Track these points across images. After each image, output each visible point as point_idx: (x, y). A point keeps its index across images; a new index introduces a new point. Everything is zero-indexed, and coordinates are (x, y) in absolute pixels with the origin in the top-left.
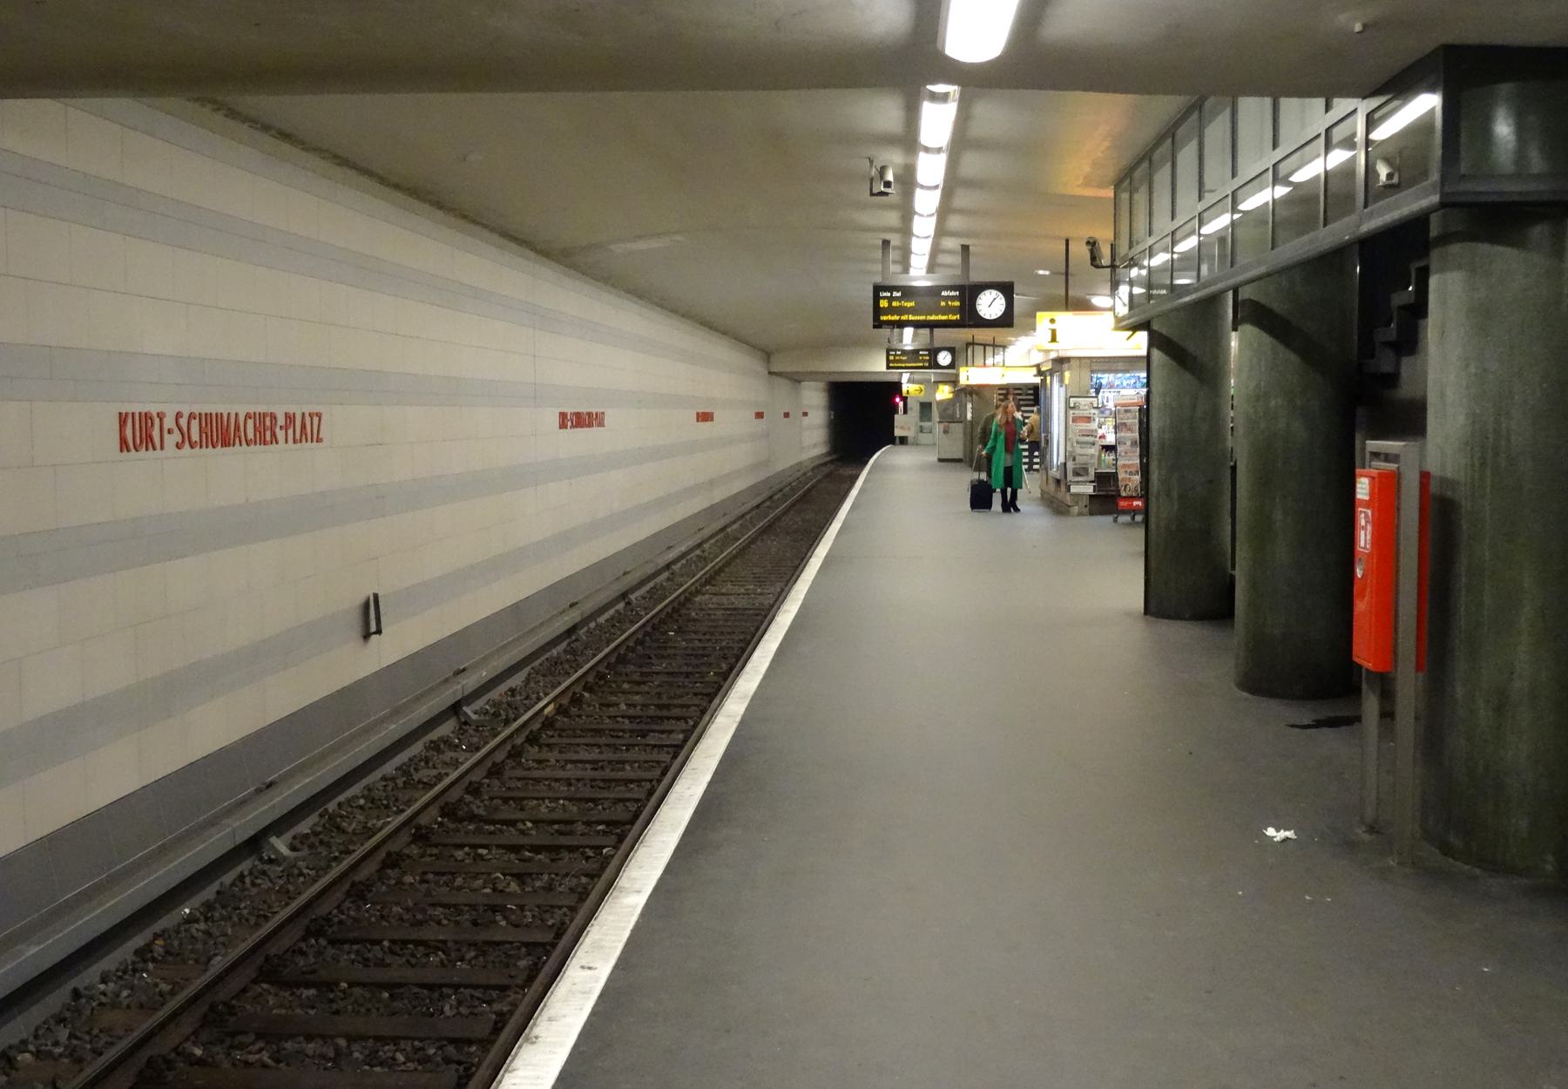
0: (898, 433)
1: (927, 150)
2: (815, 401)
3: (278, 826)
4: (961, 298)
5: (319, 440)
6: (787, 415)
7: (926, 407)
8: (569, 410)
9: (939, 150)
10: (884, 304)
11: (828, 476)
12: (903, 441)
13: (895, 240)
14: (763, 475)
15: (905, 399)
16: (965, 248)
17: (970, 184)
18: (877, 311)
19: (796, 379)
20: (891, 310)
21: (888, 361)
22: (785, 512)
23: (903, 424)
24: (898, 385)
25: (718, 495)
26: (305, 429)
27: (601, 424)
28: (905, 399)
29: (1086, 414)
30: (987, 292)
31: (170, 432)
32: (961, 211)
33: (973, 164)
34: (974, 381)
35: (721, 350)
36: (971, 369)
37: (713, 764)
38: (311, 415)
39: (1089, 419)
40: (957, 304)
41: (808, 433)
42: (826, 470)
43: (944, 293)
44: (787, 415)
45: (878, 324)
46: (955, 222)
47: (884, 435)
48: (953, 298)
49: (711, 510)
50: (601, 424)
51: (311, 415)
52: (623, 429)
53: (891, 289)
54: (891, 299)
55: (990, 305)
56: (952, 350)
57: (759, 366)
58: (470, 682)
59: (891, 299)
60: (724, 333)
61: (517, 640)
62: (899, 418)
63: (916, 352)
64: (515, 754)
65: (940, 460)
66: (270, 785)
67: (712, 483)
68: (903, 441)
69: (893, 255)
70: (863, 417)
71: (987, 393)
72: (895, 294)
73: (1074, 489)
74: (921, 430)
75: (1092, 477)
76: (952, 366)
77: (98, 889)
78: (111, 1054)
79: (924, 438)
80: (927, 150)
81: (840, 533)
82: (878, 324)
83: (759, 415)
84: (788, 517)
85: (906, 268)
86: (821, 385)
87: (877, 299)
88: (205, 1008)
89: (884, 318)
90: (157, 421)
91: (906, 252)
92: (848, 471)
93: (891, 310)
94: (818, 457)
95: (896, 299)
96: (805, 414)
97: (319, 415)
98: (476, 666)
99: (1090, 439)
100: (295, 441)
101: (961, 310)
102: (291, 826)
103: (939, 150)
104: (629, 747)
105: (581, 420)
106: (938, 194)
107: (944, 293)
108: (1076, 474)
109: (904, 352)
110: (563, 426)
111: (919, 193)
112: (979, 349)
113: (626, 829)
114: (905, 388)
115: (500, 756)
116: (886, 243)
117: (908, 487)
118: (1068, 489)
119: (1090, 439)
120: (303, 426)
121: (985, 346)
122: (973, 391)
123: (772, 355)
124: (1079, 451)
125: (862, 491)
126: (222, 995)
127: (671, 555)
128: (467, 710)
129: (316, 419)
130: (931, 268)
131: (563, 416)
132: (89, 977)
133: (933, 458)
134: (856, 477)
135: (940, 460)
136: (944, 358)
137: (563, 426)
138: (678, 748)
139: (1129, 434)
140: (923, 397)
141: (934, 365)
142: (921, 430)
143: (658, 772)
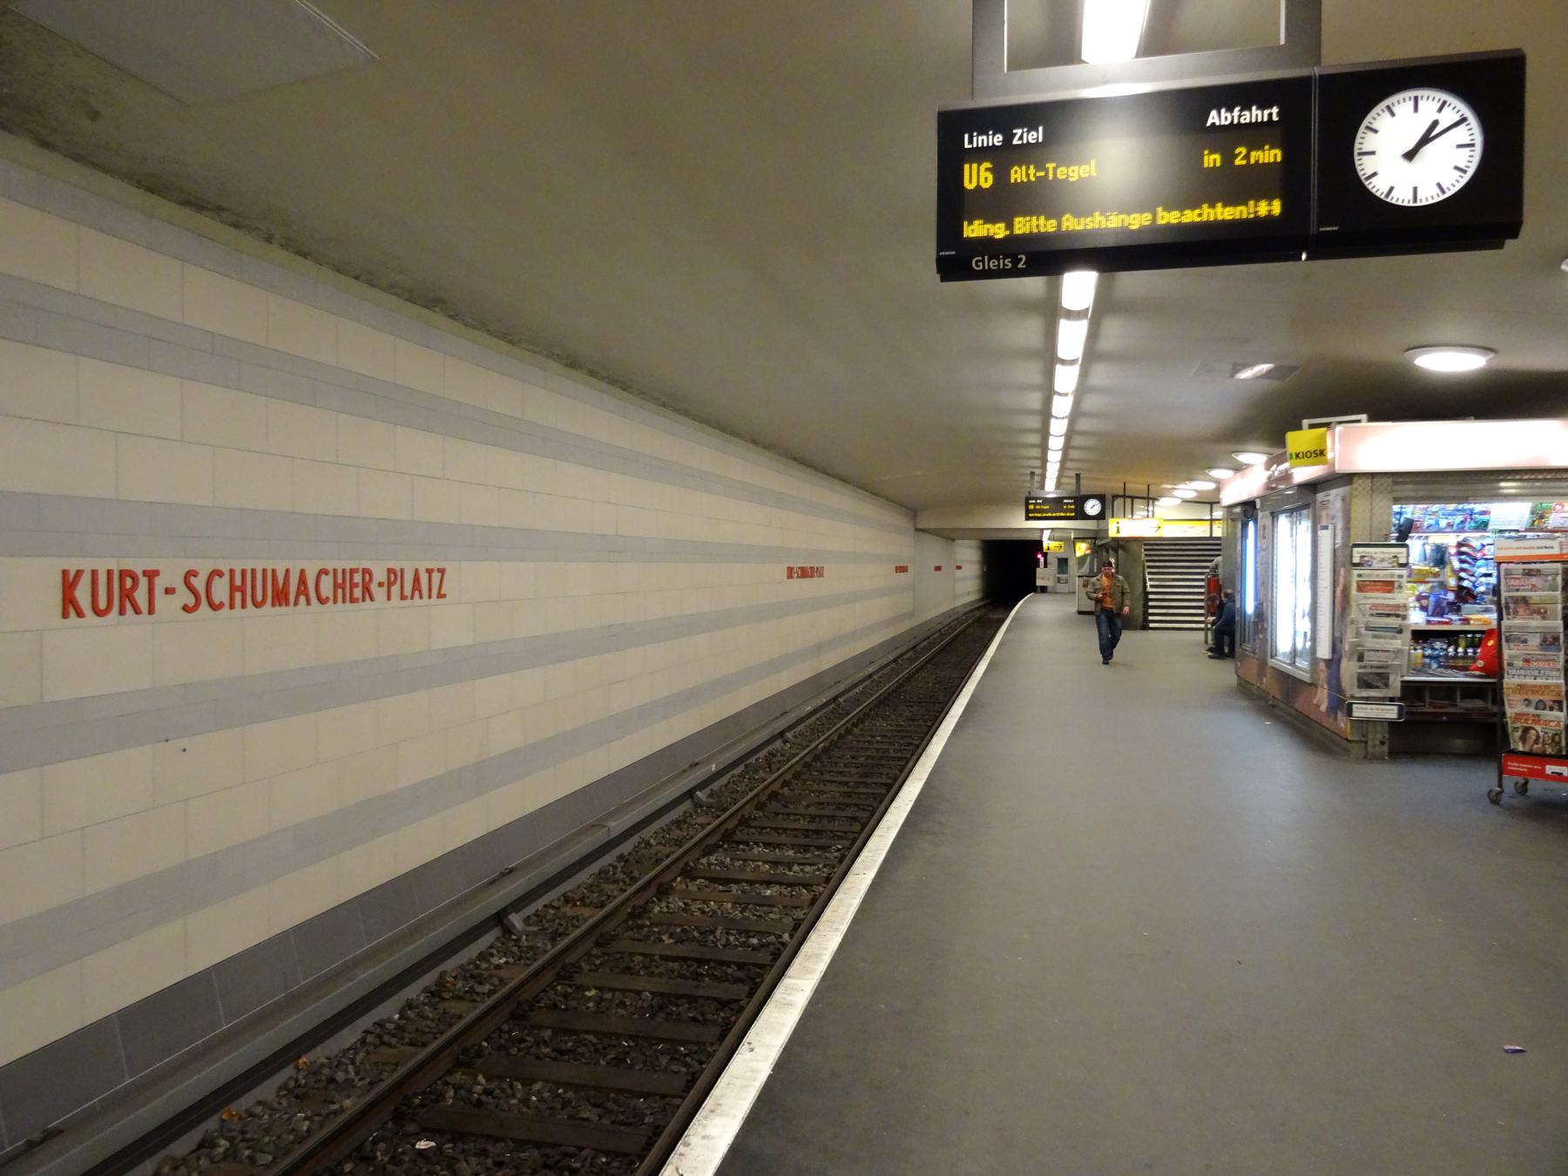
0: (1039, 583)
1: (1063, 362)
2: (969, 559)
3: (701, 786)
4: (1287, 133)
5: (440, 596)
6: (938, 569)
7: (1063, 563)
8: (795, 565)
9: (1073, 362)
10: (978, 177)
11: (979, 620)
12: (1044, 589)
13: (1038, 471)
14: (906, 626)
15: (1045, 555)
16: (1078, 476)
17: (1088, 415)
18: (953, 203)
19: (949, 537)
20: (1035, 511)
21: (1028, 511)
22: (921, 668)
23: (1043, 576)
24: (1040, 542)
25: (828, 661)
26: (422, 586)
27: (821, 575)
28: (1045, 555)
29: (1383, 576)
30: (1402, 103)
31: (169, 591)
32: (1078, 448)
33: (1102, 374)
34: (1124, 534)
35: (868, 509)
36: (1122, 521)
37: (855, 903)
38: (430, 572)
39: (1389, 586)
40: (1270, 155)
41: (962, 582)
42: (978, 614)
43: (1216, 118)
44: (938, 569)
45: (958, 261)
46: (1073, 454)
47: (1027, 585)
48: (1253, 135)
49: (817, 681)
50: (821, 575)
51: (430, 572)
52: (837, 579)
53: (1006, 118)
54: (1002, 158)
55: (1416, 152)
56: (1101, 498)
57: (898, 519)
58: (842, 687)
59: (1002, 158)
60: (844, 480)
61: (669, 781)
62: (1040, 571)
63: (1059, 500)
64: (841, 737)
65: (1080, 613)
66: (50, 1135)
67: (819, 648)
68: (1044, 589)
69: (1037, 478)
70: (1011, 570)
71: (1134, 547)
72: (1022, 136)
73: (1360, 711)
74: (1059, 580)
75: (1395, 689)
76: (1101, 516)
77: (657, 788)
78: (577, 932)
79: (1061, 587)
80: (1063, 362)
81: (958, 726)
82: (958, 261)
83: (902, 569)
84: (918, 678)
85: (1042, 487)
86: (974, 543)
87: (951, 160)
88: (559, 966)
89: (975, 230)
90: (143, 581)
91: (1043, 477)
92: (996, 616)
93: (1035, 511)
94: (971, 603)
95: (1026, 154)
96: (959, 568)
97: (442, 571)
98: (709, 760)
99: (1394, 622)
100: (403, 597)
101: (1286, 180)
102: (437, 965)
103: (1073, 362)
104: (832, 818)
105: (805, 573)
106: (1066, 422)
107: (1216, 118)
108: (1364, 683)
109: (1046, 501)
110: (790, 576)
111: (1059, 368)
112: (1128, 501)
113: (779, 959)
114: (1045, 546)
115: (798, 768)
116: (1033, 474)
117: (1046, 623)
118: (1349, 713)
119: (1394, 622)
120: (417, 580)
121: (1133, 498)
122: (1121, 545)
123: (921, 514)
124: (1370, 642)
125: (1277, 24)
126: (572, 958)
127: (871, 670)
128: (516, 920)
129: (436, 576)
130: (1058, 485)
131: (790, 570)
132: (647, 833)
133: (1074, 609)
134: (1003, 621)
135: (1080, 613)
136: (1092, 507)
137: (790, 576)
138: (889, 786)
139: (1536, 623)
140: (1062, 553)
141: (1081, 515)
142: (1059, 580)
143: (717, 1031)
